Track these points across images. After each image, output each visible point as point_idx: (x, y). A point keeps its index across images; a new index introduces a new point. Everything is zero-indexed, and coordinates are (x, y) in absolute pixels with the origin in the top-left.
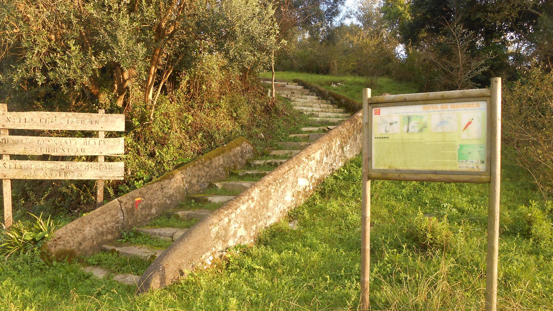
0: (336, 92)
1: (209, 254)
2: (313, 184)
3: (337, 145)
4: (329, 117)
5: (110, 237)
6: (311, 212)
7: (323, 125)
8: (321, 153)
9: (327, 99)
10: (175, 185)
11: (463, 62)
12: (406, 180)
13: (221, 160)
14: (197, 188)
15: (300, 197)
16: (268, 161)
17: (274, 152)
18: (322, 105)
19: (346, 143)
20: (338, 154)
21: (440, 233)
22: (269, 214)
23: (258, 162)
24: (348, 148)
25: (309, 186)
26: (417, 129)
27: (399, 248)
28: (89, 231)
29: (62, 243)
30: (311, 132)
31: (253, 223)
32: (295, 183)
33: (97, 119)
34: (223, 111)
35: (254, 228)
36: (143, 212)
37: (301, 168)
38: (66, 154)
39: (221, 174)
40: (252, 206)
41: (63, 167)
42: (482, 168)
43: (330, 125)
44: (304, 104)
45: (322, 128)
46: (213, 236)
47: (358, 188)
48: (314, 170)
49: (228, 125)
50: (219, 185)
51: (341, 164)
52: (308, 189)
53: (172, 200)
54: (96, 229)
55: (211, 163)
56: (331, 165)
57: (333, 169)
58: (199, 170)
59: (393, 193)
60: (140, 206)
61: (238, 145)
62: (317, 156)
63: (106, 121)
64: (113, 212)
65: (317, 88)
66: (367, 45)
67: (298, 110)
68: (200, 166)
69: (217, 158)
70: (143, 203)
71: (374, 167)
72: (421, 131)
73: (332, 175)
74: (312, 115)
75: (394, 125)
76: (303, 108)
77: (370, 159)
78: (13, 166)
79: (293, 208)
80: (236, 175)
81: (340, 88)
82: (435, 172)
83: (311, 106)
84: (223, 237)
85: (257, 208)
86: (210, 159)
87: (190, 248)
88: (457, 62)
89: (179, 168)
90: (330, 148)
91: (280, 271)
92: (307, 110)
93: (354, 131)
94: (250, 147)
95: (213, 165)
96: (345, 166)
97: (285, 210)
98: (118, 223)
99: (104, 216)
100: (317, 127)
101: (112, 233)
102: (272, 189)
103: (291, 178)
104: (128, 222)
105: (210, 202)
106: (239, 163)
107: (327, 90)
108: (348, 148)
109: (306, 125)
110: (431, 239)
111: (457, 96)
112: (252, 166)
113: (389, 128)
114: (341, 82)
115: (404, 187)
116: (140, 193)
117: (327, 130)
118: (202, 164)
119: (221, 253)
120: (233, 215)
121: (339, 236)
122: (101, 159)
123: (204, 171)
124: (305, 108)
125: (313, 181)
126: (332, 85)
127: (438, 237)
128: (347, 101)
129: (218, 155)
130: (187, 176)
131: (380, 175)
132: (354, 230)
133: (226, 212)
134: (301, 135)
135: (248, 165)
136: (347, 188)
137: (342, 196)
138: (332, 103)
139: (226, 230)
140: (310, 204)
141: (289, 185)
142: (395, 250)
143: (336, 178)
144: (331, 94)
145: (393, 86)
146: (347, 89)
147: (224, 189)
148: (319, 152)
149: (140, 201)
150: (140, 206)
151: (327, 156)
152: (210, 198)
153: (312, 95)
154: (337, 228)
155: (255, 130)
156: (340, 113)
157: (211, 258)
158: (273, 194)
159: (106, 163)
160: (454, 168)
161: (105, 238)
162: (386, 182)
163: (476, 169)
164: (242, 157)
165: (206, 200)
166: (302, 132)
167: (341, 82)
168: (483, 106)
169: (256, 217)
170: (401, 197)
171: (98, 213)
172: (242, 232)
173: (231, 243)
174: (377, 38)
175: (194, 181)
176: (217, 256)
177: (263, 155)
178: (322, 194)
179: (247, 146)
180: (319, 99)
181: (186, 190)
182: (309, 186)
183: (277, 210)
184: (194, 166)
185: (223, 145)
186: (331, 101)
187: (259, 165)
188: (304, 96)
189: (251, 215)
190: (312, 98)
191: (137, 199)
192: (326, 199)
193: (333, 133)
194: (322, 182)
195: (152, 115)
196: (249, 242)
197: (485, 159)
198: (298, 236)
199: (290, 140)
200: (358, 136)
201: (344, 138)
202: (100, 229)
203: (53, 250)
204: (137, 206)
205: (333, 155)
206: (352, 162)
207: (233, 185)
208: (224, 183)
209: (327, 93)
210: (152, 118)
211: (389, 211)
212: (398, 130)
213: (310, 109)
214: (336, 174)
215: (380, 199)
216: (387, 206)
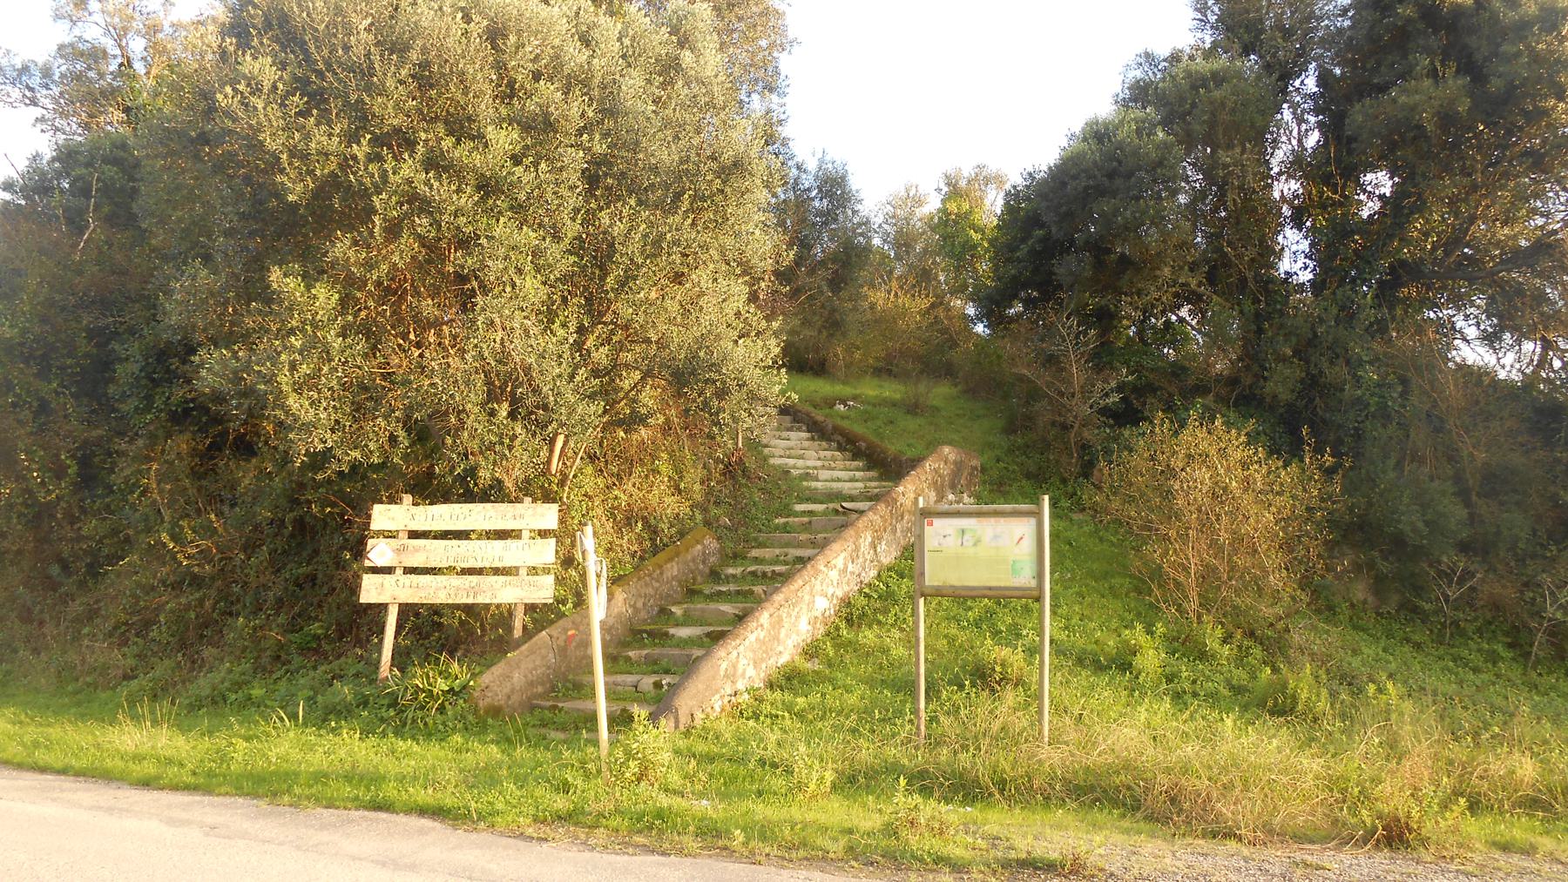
0: (845, 424)
1: (717, 697)
2: (834, 605)
3: (867, 544)
4: (839, 480)
5: (540, 689)
6: (837, 646)
7: (832, 501)
8: (845, 558)
9: (829, 440)
10: (616, 610)
11: (1082, 383)
12: (973, 598)
13: (675, 569)
14: (643, 615)
15: (818, 625)
16: (749, 569)
17: (755, 553)
18: (822, 453)
19: (880, 539)
20: (868, 557)
21: (1012, 665)
22: (781, 648)
23: (731, 571)
24: (883, 547)
25: (829, 609)
26: (971, 543)
27: (961, 687)
28: (518, 678)
29: (490, 694)
30: (811, 513)
31: (763, 660)
32: (811, 603)
33: (523, 512)
34: (661, 485)
35: (764, 666)
36: (578, 653)
37: (818, 582)
38: (478, 565)
39: (675, 592)
40: (762, 637)
41: (472, 585)
42: (1033, 583)
43: (846, 501)
44: (788, 453)
45: (831, 506)
46: (722, 673)
47: (901, 611)
48: (835, 584)
49: (672, 505)
50: (677, 610)
51: (873, 573)
52: (827, 613)
53: (612, 635)
54: (525, 676)
55: (661, 573)
56: (859, 575)
57: (861, 582)
58: (646, 585)
59: (954, 617)
60: (574, 644)
61: (698, 542)
62: (839, 562)
63: (534, 515)
64: (543, 651)
65: (808, 414)
66: (904, 313)
67: (779, 466)
68: (647, 578)
69: (669, 566)
70: (577, 639)
71: (927, 584)
72: (975, 545)
73: (860, 591)
74: (807, 476)
75: (948, 538)
76: (787, 460)
77: (923, 574)
78: (408, 584)
79: (809, 641)
80: (700, 592)
81: (852, 414)
82: (990, 588)
83: (801, 457)
84: (731, 676)
85: (767, 639)
86: (660, 567)
87: (701, 686)
88: (1071, 383)
89: (620, 583)
90: (857, 549)
91: (810, 717)
92: (797, 466)
93: (892, 518)
94: (715, 545)
95: (665, 576)
96: (879, 575)
97: (799, 644)
98: (549, 668)
99: (533, 657)
100: (821, 503)
101: (543, 684)
102: (783, 612)
103: (807, 597)
104: (560, 667)
105: (673, 635)
106: (701, 573)
107: (828, 421)
108: (883, 547)
109: (801, 500)
110: (1001, 673)
111: (1008, 510)
112: (723, 577)
113: (942, 541)
114: (854, 398)
115: (970, 608)
116: (573, 623)
117: (841, 509)
118: (650, 575)
119: (729, 698)
120: (742, 648)
121: (880, 677)
122: (523, 572)
123: (653, 588)
124: (791, 462)
125: (835, 602)
126: (838, 406)
127: (1009, 670)
128: (871, 446)
129: (671, 560)
130: (630, 596)
131: (934, 591)
132: (900, 668)
133: (733, 643)
134: (796, 519)
135: (715, 575)
136: (886, 612)
137: (879, 623)
138: (840, 448)
139: (735, 667)
140: (832, 634)
141: (805, 607)
142: (956, 688)
143: (867, 595)
144: (836, 429)
145: (960, 408)
146: (867, 418)
147: (686, 613)
148: (843, 555)
149: (573, 635)
150: (574, 644)
151: (853, 562)
152: (672, 631)
153: (799, 429)
154: (876, 667)
155: (714, 511)
156: (858, 470)
157: (720, 703)
158: (785, 620)
159: (530, 577)
160: (1008, 584)
161: (535, 690)
162: (945, 603)
163: (1029, 586)
164: (704, 562)
165: (666, 634)
166: (796, 514)
167: (854, 398)
168: (1033, 521)
169: (766, 652)
170: (966, 624)
171: (526, 653)
172: (751, 672)
173: (741, 686)
174: (927, 296)
175: (640, 604)
176: (726, 699)
177: (736, 557)
178: (849, 621)
179: (711, 543)
180: (812, 439)
181: (630, 619)
182: (829, 609)
183: (790, 643)
184: (639, 579)
185: (675, 542)
186: (838, 443)
187: (734, 576)
188: (785, 434)
189: (760, 648)
190: (799, 437)
191: (570, 633)
192: (855, 628)
193: (860, 524)
194: (847, 603)
195: (565, 495)
196: (759, 684)
197: (1035, 575)
198: (819, 678)
199: (777, 528)
200: (898, 526)
201: (876, 531)
202: (530, 675)
203: (481, 704)
204: (571, 642)
205: (861, 560)
206: (889, 569)
207: (703, 610)
208: (685, 606)
209: (830, 426)
210: (565, 500)
211: (949, 643)
212: (952, 542)
213: (800, 463)
214: (867, 590)
215: (935, 626)
216: (946, 636)
